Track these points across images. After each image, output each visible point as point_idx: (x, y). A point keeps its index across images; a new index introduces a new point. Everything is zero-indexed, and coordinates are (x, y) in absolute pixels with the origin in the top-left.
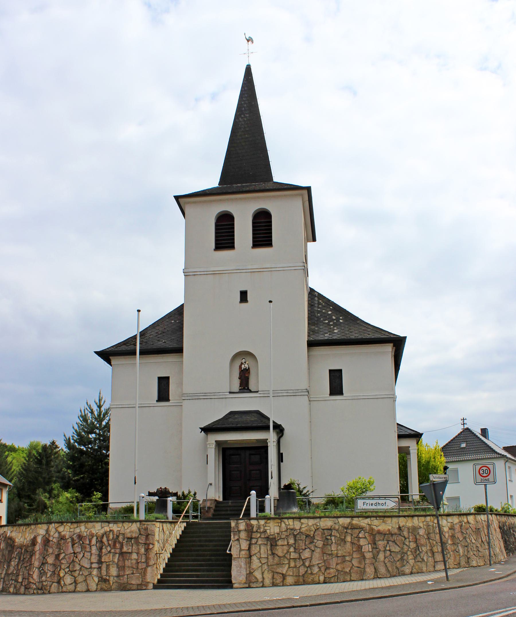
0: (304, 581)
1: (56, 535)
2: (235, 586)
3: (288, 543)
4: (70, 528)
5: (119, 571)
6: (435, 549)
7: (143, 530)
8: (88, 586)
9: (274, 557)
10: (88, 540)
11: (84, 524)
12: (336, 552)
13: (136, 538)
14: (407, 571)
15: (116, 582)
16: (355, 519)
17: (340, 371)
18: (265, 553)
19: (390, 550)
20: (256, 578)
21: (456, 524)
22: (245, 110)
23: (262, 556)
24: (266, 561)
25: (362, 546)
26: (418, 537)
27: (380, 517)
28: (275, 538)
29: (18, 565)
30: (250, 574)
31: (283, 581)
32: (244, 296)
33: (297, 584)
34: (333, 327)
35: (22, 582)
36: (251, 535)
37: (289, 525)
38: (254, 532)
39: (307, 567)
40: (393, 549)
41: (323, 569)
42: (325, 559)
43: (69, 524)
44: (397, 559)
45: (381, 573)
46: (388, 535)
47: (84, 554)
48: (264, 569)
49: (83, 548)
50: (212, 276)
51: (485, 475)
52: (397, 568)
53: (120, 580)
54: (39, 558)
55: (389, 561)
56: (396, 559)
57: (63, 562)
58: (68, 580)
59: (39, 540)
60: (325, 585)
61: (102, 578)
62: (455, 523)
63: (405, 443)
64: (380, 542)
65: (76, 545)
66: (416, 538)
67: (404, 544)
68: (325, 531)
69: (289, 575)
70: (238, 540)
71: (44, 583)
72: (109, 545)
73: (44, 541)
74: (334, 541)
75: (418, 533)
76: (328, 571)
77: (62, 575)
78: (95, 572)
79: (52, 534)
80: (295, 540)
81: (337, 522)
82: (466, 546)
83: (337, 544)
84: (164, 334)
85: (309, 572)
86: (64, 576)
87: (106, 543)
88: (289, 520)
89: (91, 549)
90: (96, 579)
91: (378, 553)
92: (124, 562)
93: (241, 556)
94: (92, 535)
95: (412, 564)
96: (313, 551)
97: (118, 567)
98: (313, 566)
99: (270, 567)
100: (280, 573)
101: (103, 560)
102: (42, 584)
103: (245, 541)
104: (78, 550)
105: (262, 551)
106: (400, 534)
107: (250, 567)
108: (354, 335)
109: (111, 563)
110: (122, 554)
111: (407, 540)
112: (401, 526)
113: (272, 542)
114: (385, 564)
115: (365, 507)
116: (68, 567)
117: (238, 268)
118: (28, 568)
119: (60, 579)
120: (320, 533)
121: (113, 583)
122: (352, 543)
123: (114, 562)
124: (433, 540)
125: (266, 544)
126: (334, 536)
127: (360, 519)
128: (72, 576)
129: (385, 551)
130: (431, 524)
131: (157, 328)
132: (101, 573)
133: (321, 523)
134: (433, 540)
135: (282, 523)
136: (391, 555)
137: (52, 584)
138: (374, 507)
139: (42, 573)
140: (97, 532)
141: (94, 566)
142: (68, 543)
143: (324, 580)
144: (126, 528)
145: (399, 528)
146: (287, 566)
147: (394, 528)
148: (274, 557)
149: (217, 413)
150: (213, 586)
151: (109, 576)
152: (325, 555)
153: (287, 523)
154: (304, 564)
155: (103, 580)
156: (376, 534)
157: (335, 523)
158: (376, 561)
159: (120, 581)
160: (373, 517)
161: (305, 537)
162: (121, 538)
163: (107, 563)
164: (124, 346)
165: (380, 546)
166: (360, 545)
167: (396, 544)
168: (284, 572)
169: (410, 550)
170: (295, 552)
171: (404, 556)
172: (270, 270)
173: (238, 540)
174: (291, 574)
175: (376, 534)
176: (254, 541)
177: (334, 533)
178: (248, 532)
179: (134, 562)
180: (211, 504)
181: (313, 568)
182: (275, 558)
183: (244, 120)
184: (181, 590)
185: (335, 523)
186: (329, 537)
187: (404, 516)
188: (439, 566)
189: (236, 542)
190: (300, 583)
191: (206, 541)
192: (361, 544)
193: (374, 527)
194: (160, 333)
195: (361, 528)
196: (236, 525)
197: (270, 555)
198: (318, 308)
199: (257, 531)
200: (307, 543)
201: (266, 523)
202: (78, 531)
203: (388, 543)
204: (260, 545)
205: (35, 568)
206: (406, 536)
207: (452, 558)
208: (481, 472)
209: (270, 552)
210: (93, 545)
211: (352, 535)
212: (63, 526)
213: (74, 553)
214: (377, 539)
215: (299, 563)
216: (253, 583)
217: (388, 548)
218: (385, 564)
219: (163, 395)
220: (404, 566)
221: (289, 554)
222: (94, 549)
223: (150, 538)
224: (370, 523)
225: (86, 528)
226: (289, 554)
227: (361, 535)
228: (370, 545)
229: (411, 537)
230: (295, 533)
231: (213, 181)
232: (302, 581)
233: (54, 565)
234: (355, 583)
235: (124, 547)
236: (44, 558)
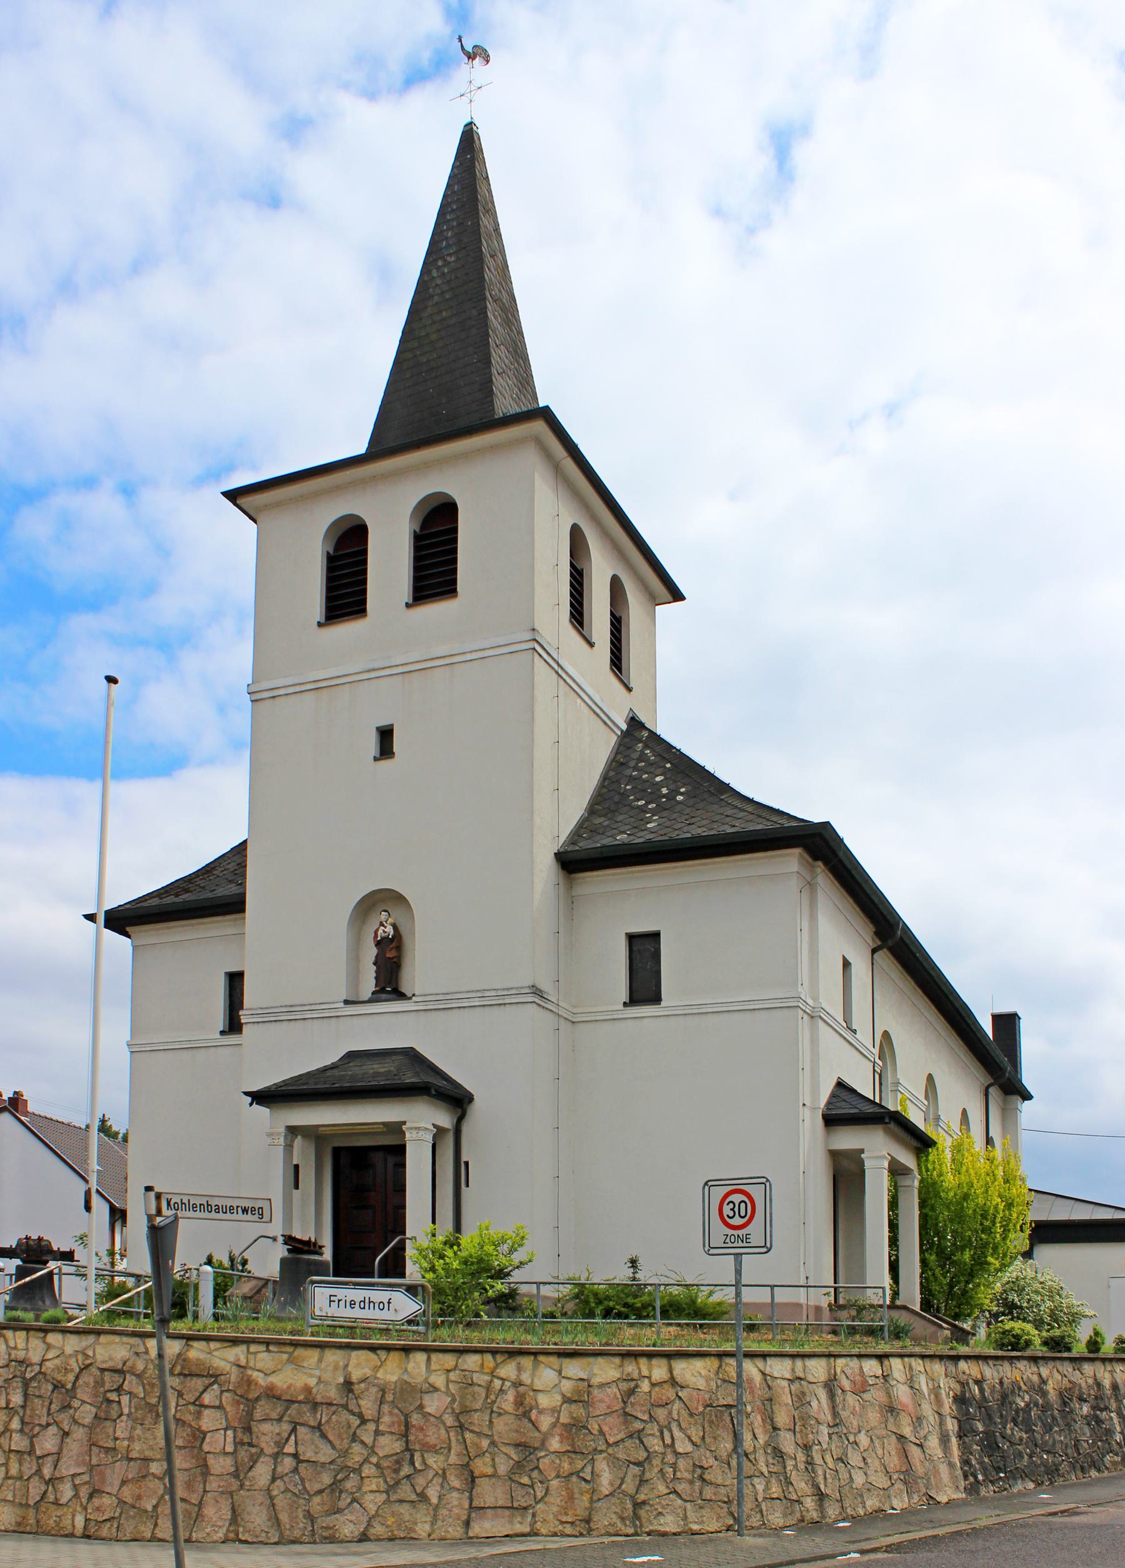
3: (8, 1402)
6: (481, 1466)
12: (126, 1443)
14: (348, 1527)
16: (195, 1344)
19: (295, 1456)
21: (602, 1386)
22: (449, 246)
25: (205, 1434)
26: (415, 1419)
37: (15, 1348)
39: (47, 1483)
40: (308, 1453)
41: (84, 1492)
42: (94, 1461)
44: (317, 1487)
45: (250, 1526)
51: (737, 1221)
52: (310, 1517)
55: (287, 1490)
62: (595, 1381)
63: (848, 1139)
64: (266, 1427)
66: (407, 1425)
67: (354, 1438)
74: (126, 1411)
75: (421, 1407)
76: (96, 1501)
80: (26, 1395)
81: (142, 1349)
82: (638, 1464)
83: (135, 1420)
95: (372, 1509)
98: (61, 1479)
106: (345, 1407)
108: (699, 829)
111: (371, 1427)
112: (354, 1378)
114: (272, 1498)
115: (334, 1310)
117: (371, 666)
120: (92, 1380)
124: (479, 1434)
126: (130, 1393)
127: (213, 1345)
129: (276, 1456)
130: (482, 1379)
133: (99, 1350)
134: (479, 1434)
136: (296, 1470)
138: (357, 1313)
145: (348, 1385)
147: (326, 1383)
152: (95, 1450)
154: (39, 1472)
156: (258, 1399)
157: (137, 1354)
158: (242, 1486)
161: (50, 1387)
165: (263, 1438)
166: (199, 1429)
167: (324, 1436)
169: (374, 1460)
170: (21, 1431)
171: (347, 1477)
172: (449, 662)
175: (258, 1399)
177: (130, 1383)
181: (61, 1487)
183: (444, 274)
185: (137, 1354)
186: (113, 1396)
187: (373, 1348)
188: (487, 1525)
190: (28, 1529)
192: (204, 1428)
193: (255, 1374)
195: (215, 1377)
198: (635, 768)
200: (53, 1406)
203: (294, 1430)
206: (369, 1414)
207: (556, 1500)
208: (727, 1210)
214: (258, 1414)
217: (290, 1448)
220: (339, 1511)
221: (8, 1434)
224: (243, 1362)
227: (207, 1399)
228: (230, 1433)
229: (386, 1419)
230: (28, 1376)
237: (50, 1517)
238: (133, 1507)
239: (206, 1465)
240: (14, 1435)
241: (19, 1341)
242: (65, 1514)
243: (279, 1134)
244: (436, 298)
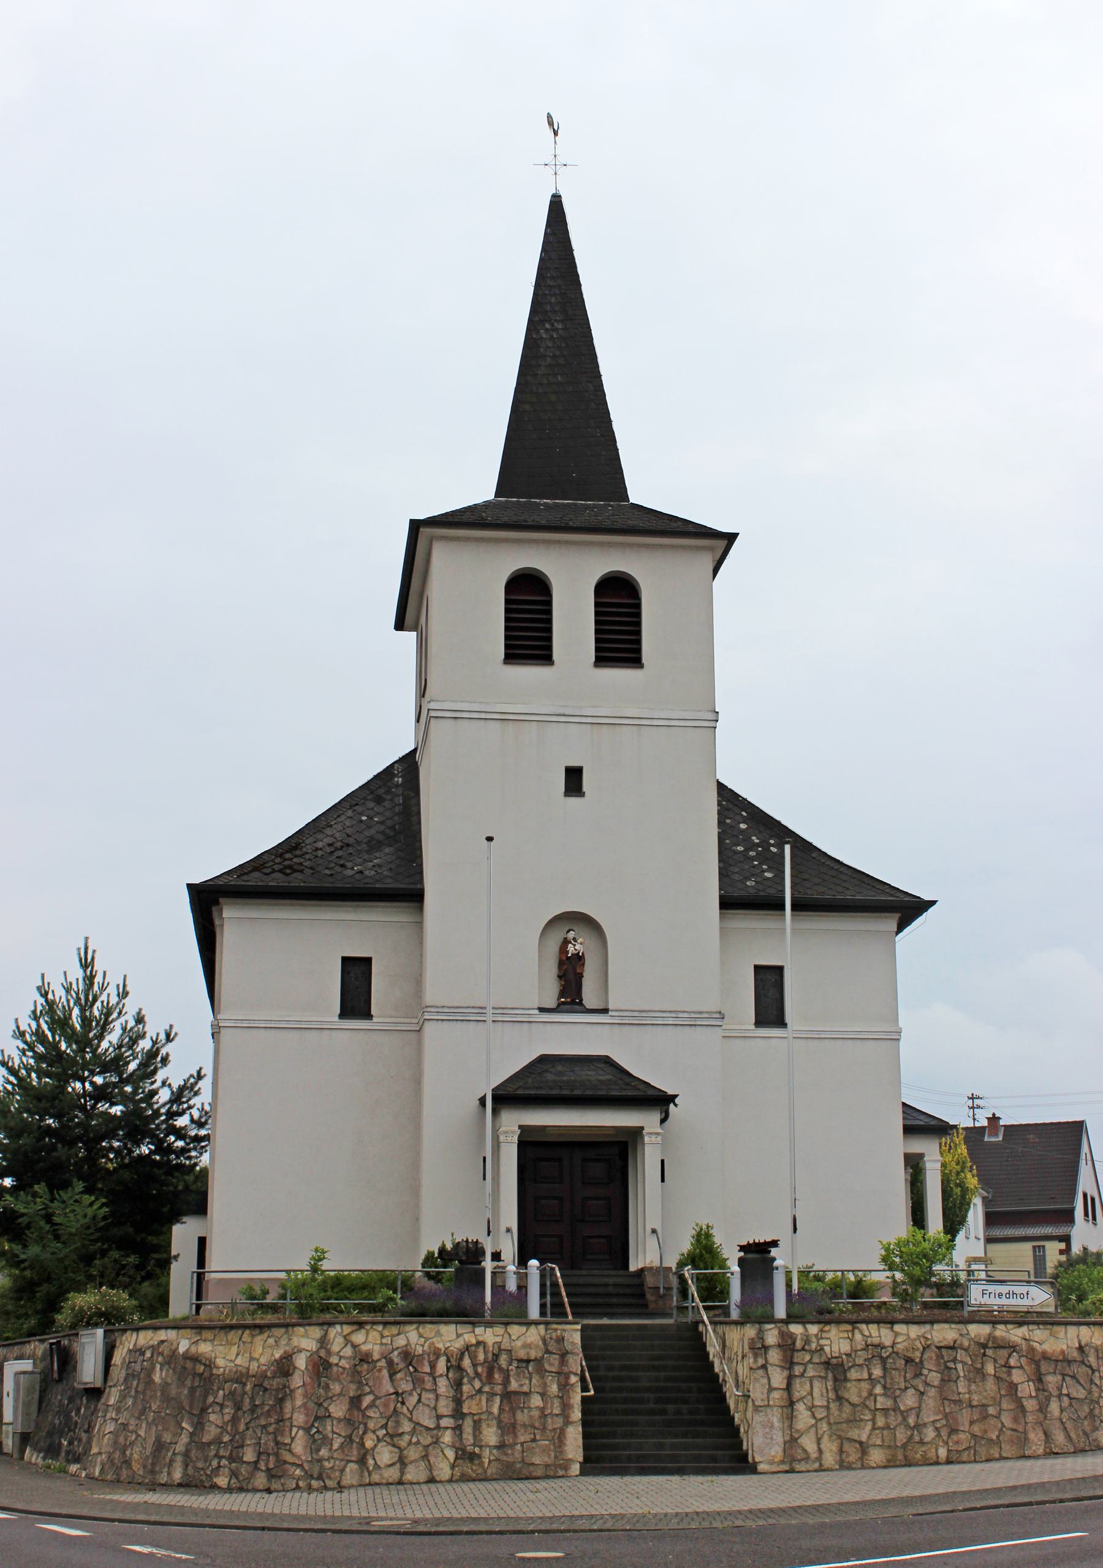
0: (906, 1457)
1: (348, 1351)
2: (761, 1467)
3: (870, 1375)
4: (382, 1337)
5: (502, 1435)
7: (552, 1342)
8: (431, 1471)
9: (841, 1404)
10: (426, 1363)
11: (415, 1326)
13: (539, 1361)
15: (497, 1460)
16: (999, 1326)
17: (780, 969)
18: (822, 1395)
19: (1068, 1395)
20: (805, 1451)
23: (817, 1403)
24: (825, 1414)
25: (1016, 1385)
27: (1045, 1323)
28: (842, 1365)
29: (235, 1420)
30: (792, 1442)
31: (861, 1459)
32: (574, 780)
33: (890, 1464)
34: (769, 870)
35: (256, 1462)
36: (792, 1357)
37: (871, 1336)
38: (798, 1351)
40: (1074, 1394)
41: (944, 1433)
42: (947, 1410)
43: (380, 1328)
46: (1062, 1361)
47: (420, 1395)
48: (820, 1432)
49: (417, 1382)
50: (497, 724)
53: (506, 1454)
54: (304, 1405)
55: (1070, 1418)
56: (1082, 1415)
57: (372, 1415)
58: (385, 1455)
59: (301, 1362)
60: (949, 1467)
61: (464, 1450)
63: (918, 1146)
65: (399, 1376)
67: (1092, 1381)
68: (944, 1351)
69: (875, 1445)
70: (764, 1367)
71: (326, 1464)
72: (477, 1374)
73: (316, 1366)
74: (962, 1374)
76: (955, 1437)
77: (369, 1444)
78: (447, 1437)
79: (335, 1348)
80: (885, 1369)
81: (965, 1332)
83: (969, 1380)
84: (351, 850)
85: (917, 1439)
86: (376, 1446)
87: (470, 1370)
88: (870, 1326)
89: (436, 1384)
90: (451, 1454)
91: (1048, 1399)
92: (514, 1415)
93: (771, 1403)
94: (437, 1354)
96: (922, 1393)
97: (499, 1427)
98: (925, 1425)
99: (834, 1428)
100: (855, 1441)
101: (465, 1411)
102: (322, 1467)
103: (778, 1369)
104: (405, 1386)
105: (816, 1392)
106: (1083, 1362)
107: (791, 1427)
109: (484, 1417)
110: (507, 1396)
111: (1097, 1374)
113: (836, 1370)
115: (986, 1300)
116: (385, 1426)
117: (561, 711)
118: (271, 1429)
119: (365, 1455)
120: (934, 1355)
121: (490, 1461)
122: (998, 1378)
123: (490, 1413)
125: (825, 1378)
126: (961, 1362)
127: (1009, 1326)
128: (394, 1446)
131: (328, 831)
132: (461, 1439)
133: (934, 1333)
135: (856, 1331)
136: (1071, 1405)
137: (345, 1467)
138: (1004, 1301)
139: (316, 1442)
140: (448, 1344)
141: (444, 1422)
142: (380, 1370)
143: (948, 1457)
144: (513, 1337)
145: (1081, 1349)
146: (869, 1425)
148: (841, 1404)
149: (511, 1059)
150: (714, 1467)
151: (481, 1447)
152: (946, 1402)
153: (867, 1333)
155: (465, 1455)
158: (1045, 1417)
159: (505, 1458)
160: (1034, 1323)
161: (903, 1362)
162: (503, 1361)
163: (476, 1418)
164: (256, 874)
166: (1012, 1382)
167: (1078, 1382)
168: (864, 1438)
170: (885, 1395)
172: (639, 723)
173: (764, 1367)
174: (879, 1442)
176: (797, 1370)
178: (785, 1351)
179: (536, 1413)
182: (844, 1409)
184: (732, 1478)
186: (951, 1365)
189: (761, 1372)
191: (624, 1368)
194: (339, 844)
195: (1013, 1348)
196: (758, 1334)
197: (833, 1401)
199: (803, 1349)
200: (908, 1375)
201: (821, 1331)
202: (401, 1341)
203: (1064, 1379)
204: (811, 1379)
205: (295, 1430)
206: (1094, 1365)
209: (831, 1395)
210: (441, 1375)
211: (995, 1361)
212: (363, 1331)
213: (396, 1393)
214: (1043, 1369)
215: (894, 1420)
216: (800, 1461)
217: (1065, 1391)
218: (1062, 1423)
219: (355, 1000)
220: (1097, 1429)
221: (872, 1398)
222: (443, 1385)
223: (571, 1360)
225: (421, 1336)
226: (872, 1398)
227: (1012, 1362)
231: (479, 485)
232: (903, 1458)
233: (348, 1421)
234: (1058, 1462)
235: (512, 1380)
236: (320, 1405)
237: (916, 1453)
238: (982, 1438)
239: (1023, 1406)
240: (878, 1398)
241: (872, 1332)
242: (929, 1449)
243: (513, 1132)
244: (549, 360)
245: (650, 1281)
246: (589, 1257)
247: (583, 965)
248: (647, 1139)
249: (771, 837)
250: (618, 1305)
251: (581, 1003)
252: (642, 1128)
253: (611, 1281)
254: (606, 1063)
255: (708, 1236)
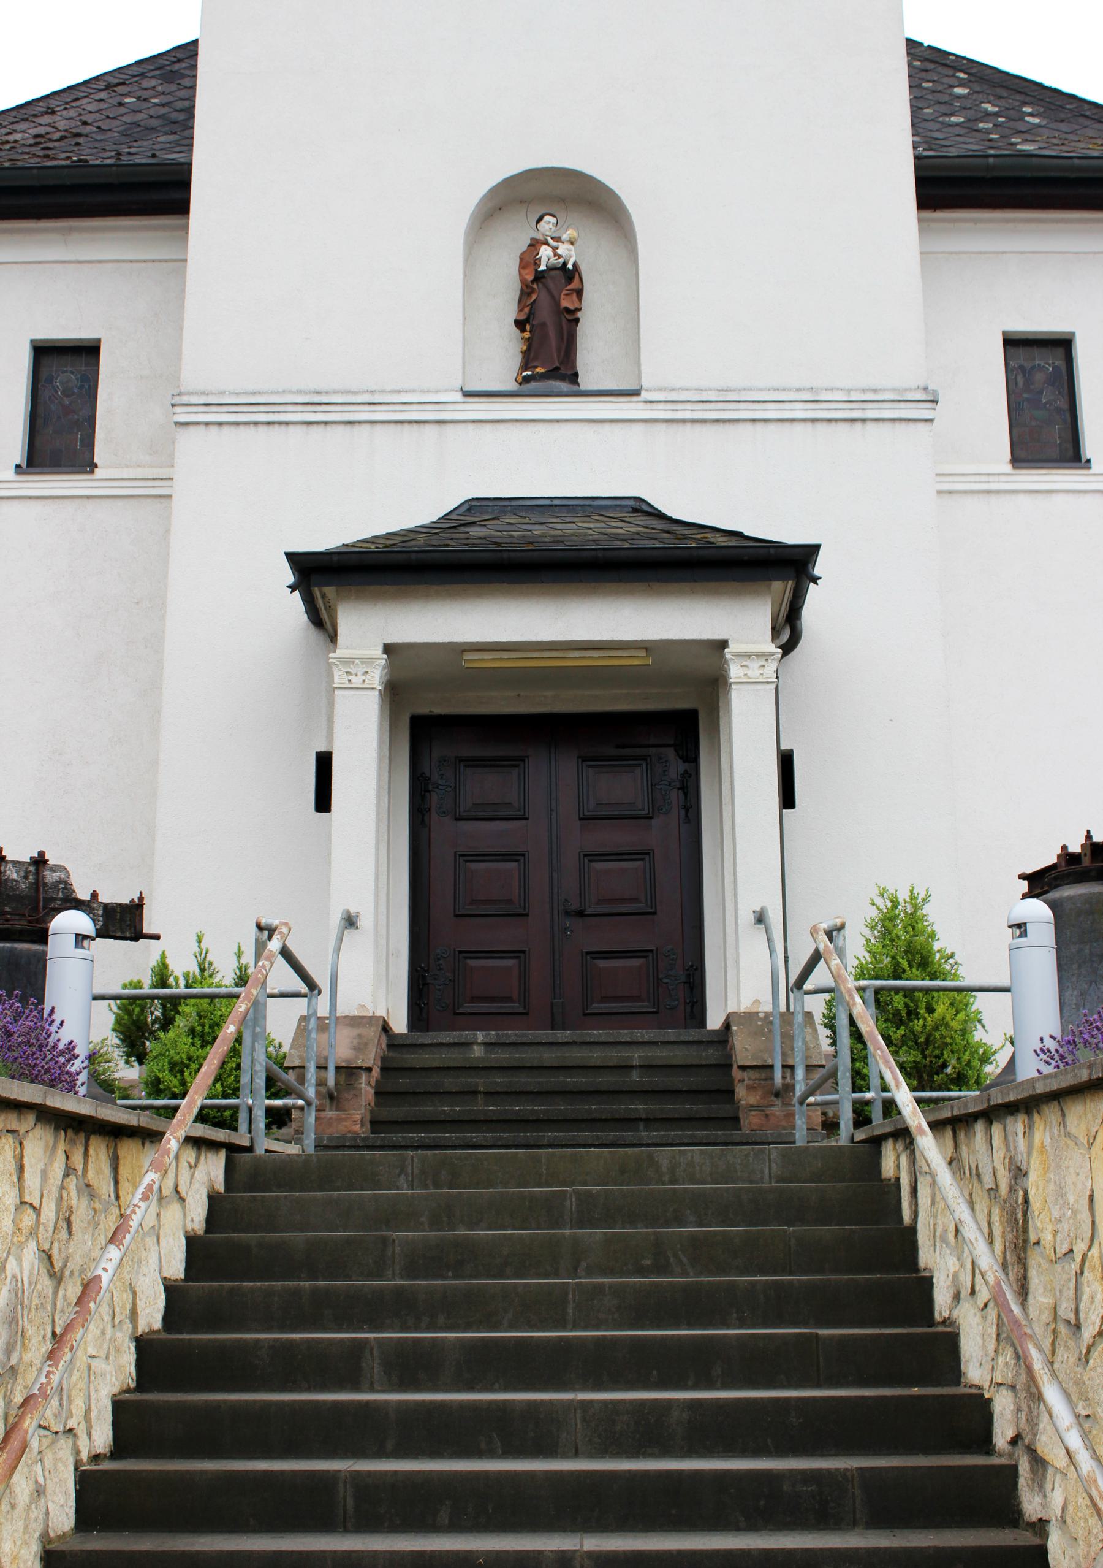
17: (1063, 345)
149: (401, 494)
180: (360, 1047)
243: (368, 661)
245: (744, 1049)
246: (596, 1007)
247: (579, 293)
248: (735, 672)
249: (1025, 104)
250: (650, 1121)
251: (574, 378)
252: (723, 644)
253: (636, 1056)
254: (635, 510)
255: (914, 921)
